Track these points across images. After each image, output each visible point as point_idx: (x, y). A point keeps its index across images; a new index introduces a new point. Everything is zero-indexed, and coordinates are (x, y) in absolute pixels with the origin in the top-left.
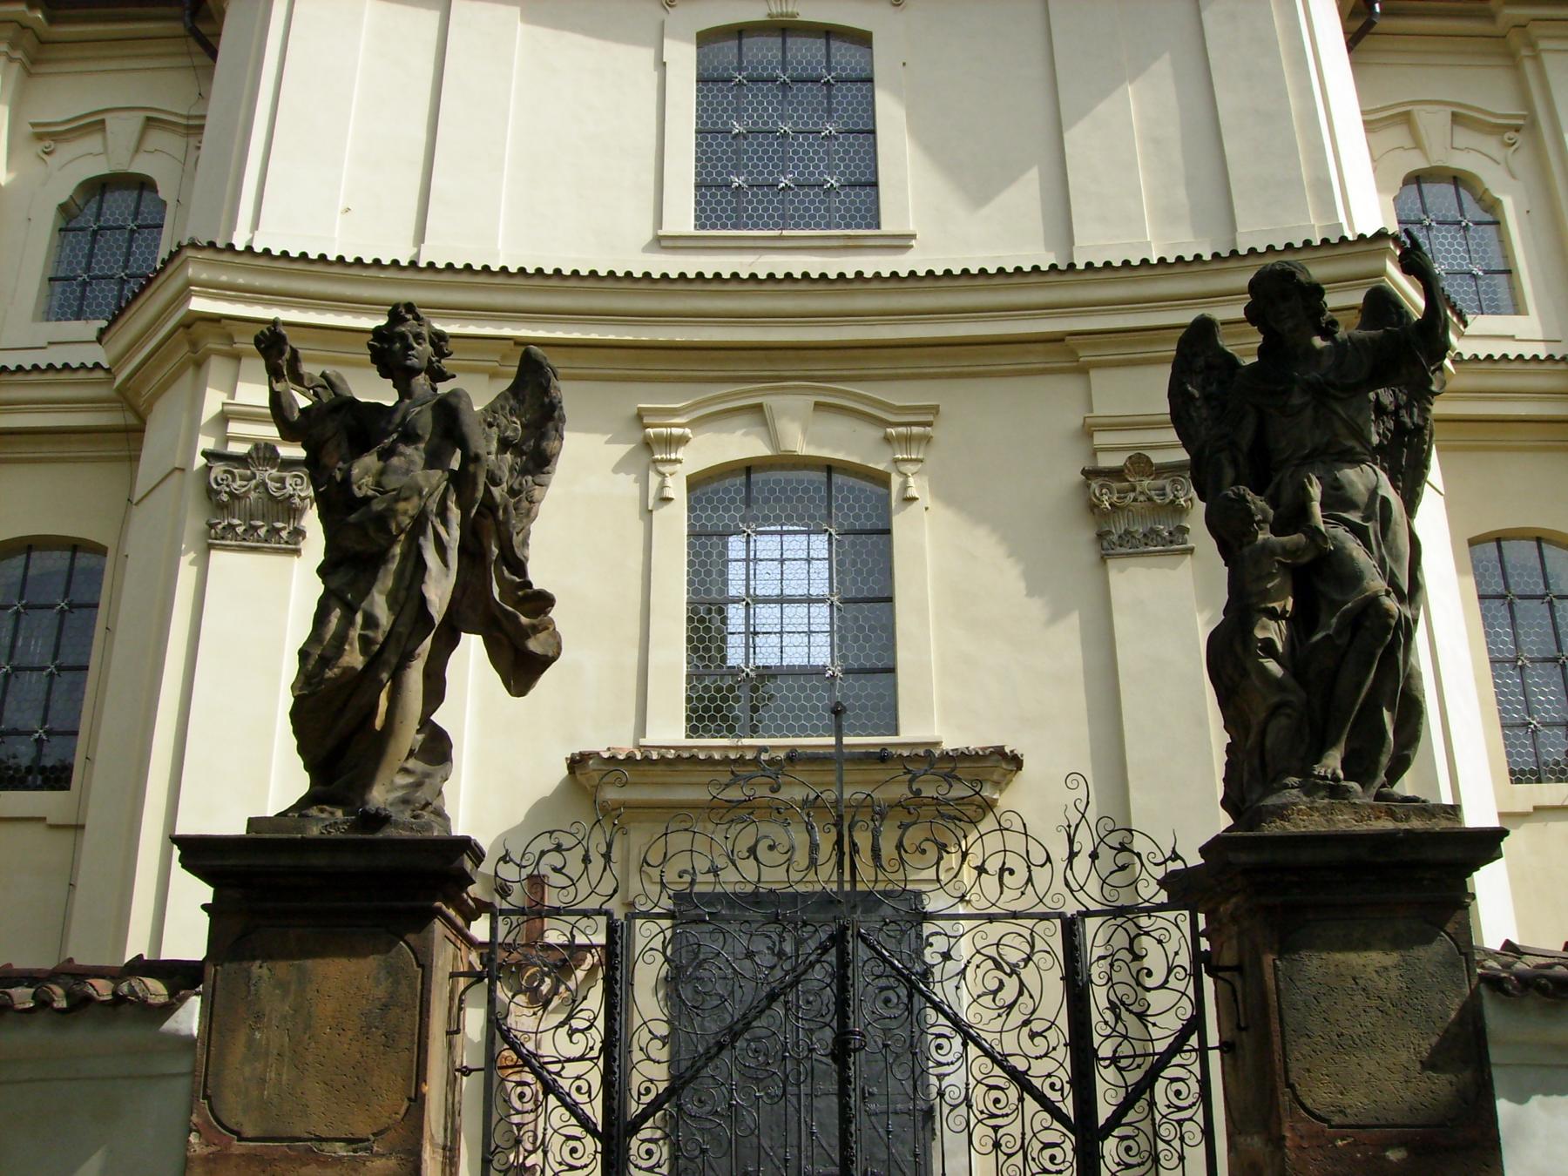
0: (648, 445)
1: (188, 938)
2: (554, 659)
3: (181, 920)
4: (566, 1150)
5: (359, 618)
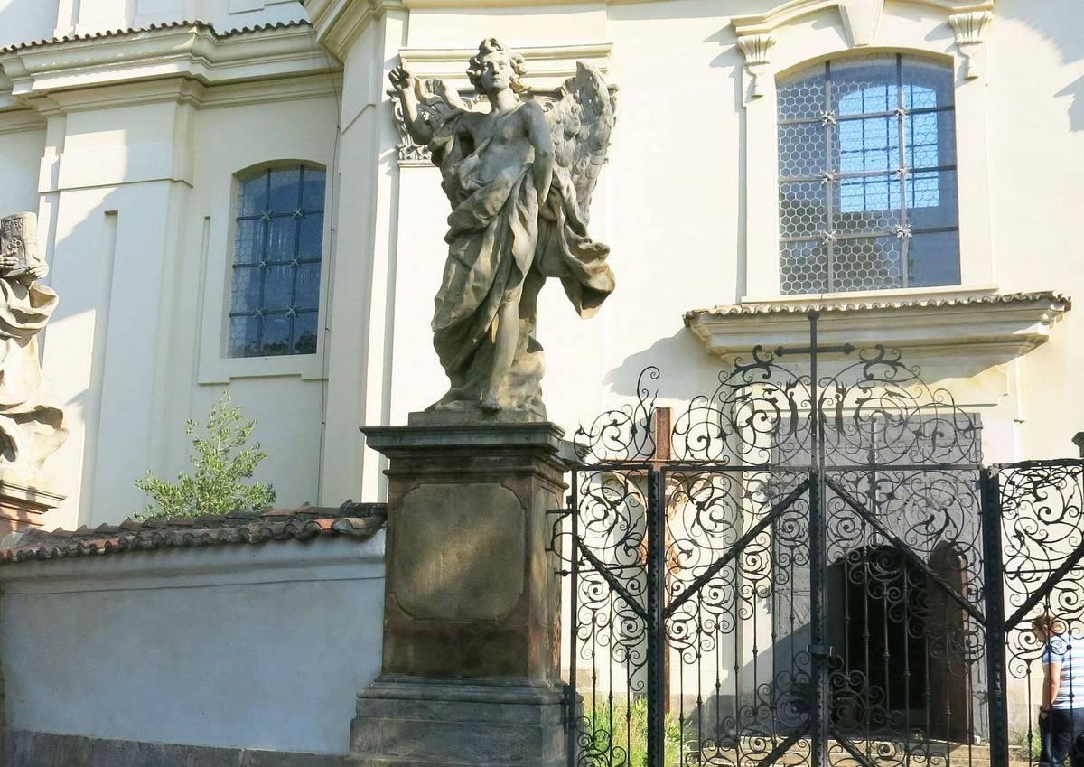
0: (740, 51)
1: (373, 490)
2: (609, 293)
3: (372, 480)
4: (625, 626)
5: (472, 274)
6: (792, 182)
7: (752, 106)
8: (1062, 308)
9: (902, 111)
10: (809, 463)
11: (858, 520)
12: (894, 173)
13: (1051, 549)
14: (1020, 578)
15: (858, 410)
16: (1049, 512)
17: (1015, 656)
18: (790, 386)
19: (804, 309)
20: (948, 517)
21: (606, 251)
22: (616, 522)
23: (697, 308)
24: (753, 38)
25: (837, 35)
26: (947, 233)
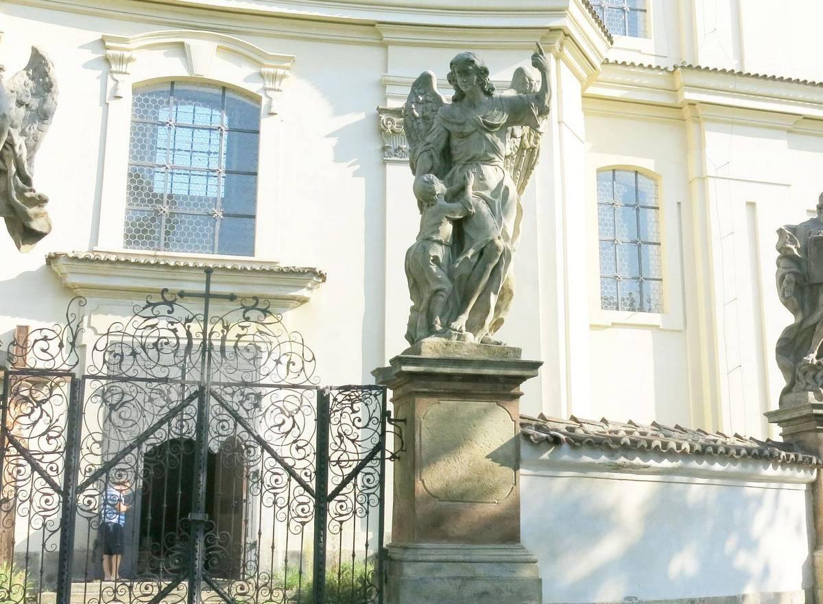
0: (107, 60)
2: (46, 234)
6: (139, 166)
7: (113, 104)
8: (321, 281)
9: (223, 128)
10: (198, 379)
11: (232, 422)
12: (214, 171)
13: (360, 446)
14: (339, 466)
15: (237, 341)
16: (360, 420)
17: (333, 519)
18: (188, 320)
19: (201, 265)
20: (294, 422)
21: (46, 201)
22: (41, 417)
23: (59, 250)
24: (118, 53)
25: (181, 63)
26: (248, 219)
